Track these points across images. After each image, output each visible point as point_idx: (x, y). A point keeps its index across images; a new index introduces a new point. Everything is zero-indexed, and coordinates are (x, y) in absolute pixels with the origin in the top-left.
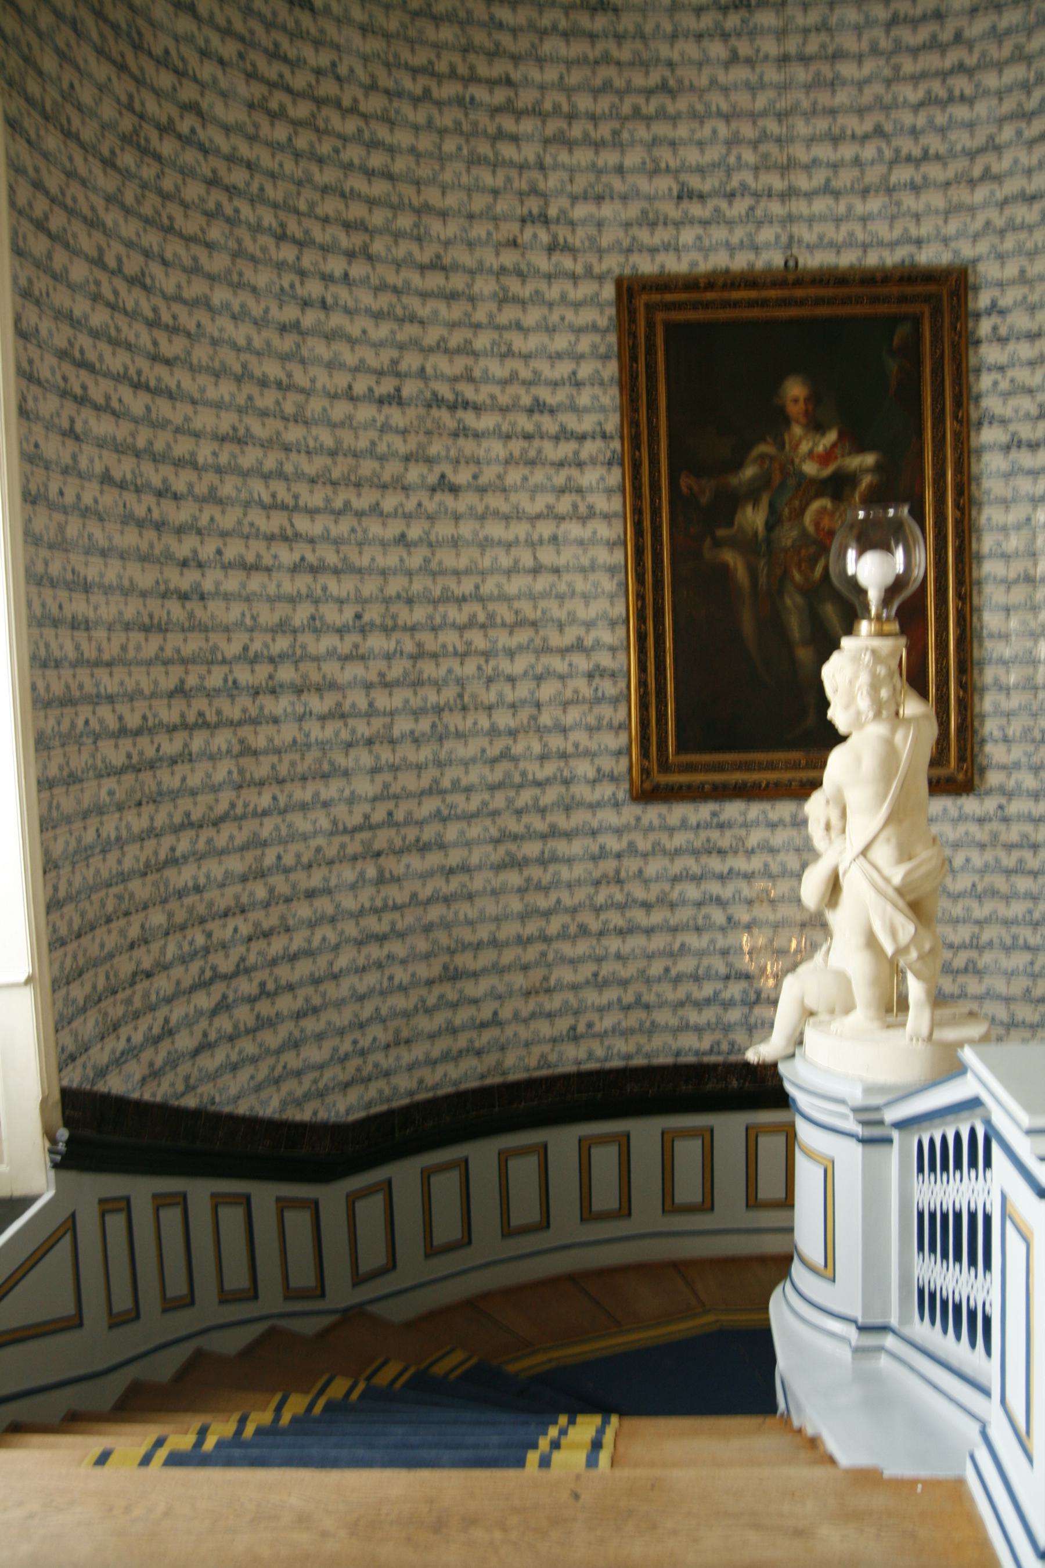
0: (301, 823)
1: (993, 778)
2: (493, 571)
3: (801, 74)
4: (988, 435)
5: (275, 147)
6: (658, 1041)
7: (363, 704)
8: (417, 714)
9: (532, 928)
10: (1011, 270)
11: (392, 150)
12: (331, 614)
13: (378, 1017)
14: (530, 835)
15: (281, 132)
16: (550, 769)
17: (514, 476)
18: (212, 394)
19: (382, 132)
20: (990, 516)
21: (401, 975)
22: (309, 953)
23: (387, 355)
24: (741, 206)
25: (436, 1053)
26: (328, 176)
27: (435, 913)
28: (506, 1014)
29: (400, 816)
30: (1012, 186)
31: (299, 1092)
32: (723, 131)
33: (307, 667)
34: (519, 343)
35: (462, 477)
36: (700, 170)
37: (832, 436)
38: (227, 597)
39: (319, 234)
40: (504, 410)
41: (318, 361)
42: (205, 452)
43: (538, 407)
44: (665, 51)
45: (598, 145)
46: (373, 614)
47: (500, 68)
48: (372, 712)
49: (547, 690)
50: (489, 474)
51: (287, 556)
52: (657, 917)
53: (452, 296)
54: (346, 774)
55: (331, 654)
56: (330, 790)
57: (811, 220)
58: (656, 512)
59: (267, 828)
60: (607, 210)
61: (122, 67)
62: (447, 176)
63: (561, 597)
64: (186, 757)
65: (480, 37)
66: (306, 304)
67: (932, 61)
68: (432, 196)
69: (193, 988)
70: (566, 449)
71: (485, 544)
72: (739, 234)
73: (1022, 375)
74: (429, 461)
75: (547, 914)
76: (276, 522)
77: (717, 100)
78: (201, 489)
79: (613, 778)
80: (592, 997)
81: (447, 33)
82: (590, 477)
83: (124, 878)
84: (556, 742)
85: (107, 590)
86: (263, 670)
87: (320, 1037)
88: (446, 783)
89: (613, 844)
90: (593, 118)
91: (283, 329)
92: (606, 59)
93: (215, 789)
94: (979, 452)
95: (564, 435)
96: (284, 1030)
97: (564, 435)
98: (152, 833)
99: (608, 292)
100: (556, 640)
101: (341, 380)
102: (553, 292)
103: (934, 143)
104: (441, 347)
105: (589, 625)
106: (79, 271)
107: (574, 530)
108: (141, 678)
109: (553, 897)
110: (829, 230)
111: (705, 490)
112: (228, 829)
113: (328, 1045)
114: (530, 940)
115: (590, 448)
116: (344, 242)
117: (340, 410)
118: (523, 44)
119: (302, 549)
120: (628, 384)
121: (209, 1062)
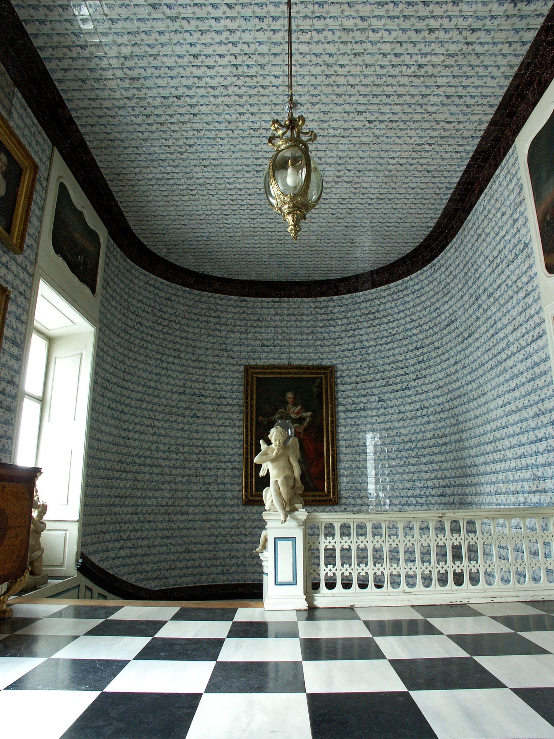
0: (149, 502)
1: (343, 501)
2: (207, 439)
3: (293, 318)
4: (340, 408)
5: (158, 331)
6: (248, 576)
7: (168, 472)
8: (183, 476)
9: (212, 540)
10: (345, 367)
11: (188, 332)
12: (162, 447)
13: (165, 561)
14: (213, 513)
15: (160, 328)
16: (220, 494)
17: (214, 415)
18: (136, 389)
19: (186, 328)
20: (341, 429)
21: (173, 549)
22: (148, 538)
23: (182, 382)
24: (277, 349)
25: (182, 574)
26: (171, 338)
27: (184, 532)
28: (203, 564)
29: (176, 504)
30: (345, 347)
31: (141, 578)
32: (273, 331)
33: (154, 460)
34: (217, 381)
35: (200, 414)
36: (267, 340)
37: (299, 407)
38: (135, 440)
39: (167, 351)
40: (213, 397)
41: (164, 382)
42: (133, 403)
43: (222, 397)
44: (259, 311)
45: (241, 333)
46: (173, 448)
47: (216, 314)
48: (171, 474)
49: (220, 473)
50: (207, 414)
51: (151, 431)
52: (248, 539)
53: (201, 368)
54: (162, 490)
55: (161, 457)
56: (158, 494)
57: (295, 353)
58: (252, 426)
59: (139, 501)
60: (243, 348)
61: (124, 315)
62: (201, 339)
63: (225, 447)
64: (120, 478)
65: (212, 307)
66: (162, 368)
67: (325, 317)
68: (197, 343)
69: (115, 541)
70: (229, 408)
71: (205, 432)
72: (277, 356)
73: (348, 393)
74: (191, 409)
75: (217, 536)
76: (149, 422)
77: (272, 323)
78: (131, 412)
79: (238, 498)
80: (228, 561)
81: (204, 306)
82: (235, 416)
83: (102, 505)
84: (221, 487)
85: (106, 433)
86: (142, 460)
87: (148, 563)
88: (190, 496)
89: (236, 516)
90: (240, 326)
91: (156, 374)
92: (244, 312)
93: (127, 488)
94: (338, 412)
95: (228, 405)
96: (139, 558)
97: (228, 405)
98: (109, 496)
99: (242, 369)
100: (223, 459)
101: (170, 388)
102: (227, 368)
103: (326, 336)
104: (197, 381)
105: (233, 455)
106: (109, 359)
107: (230, 430)
108: (111, 456)
109: (219, 531)
110: (300, 355)
111: (265, 420)
112: (129, 500)
113: (150, 565)
114: (211, 543)
115: (235, 408)
116: (174, 354)
117: (169, 395)
118: (224, 308)
119: (156, 430)
120: (246, 392)
121: (118, 562)
